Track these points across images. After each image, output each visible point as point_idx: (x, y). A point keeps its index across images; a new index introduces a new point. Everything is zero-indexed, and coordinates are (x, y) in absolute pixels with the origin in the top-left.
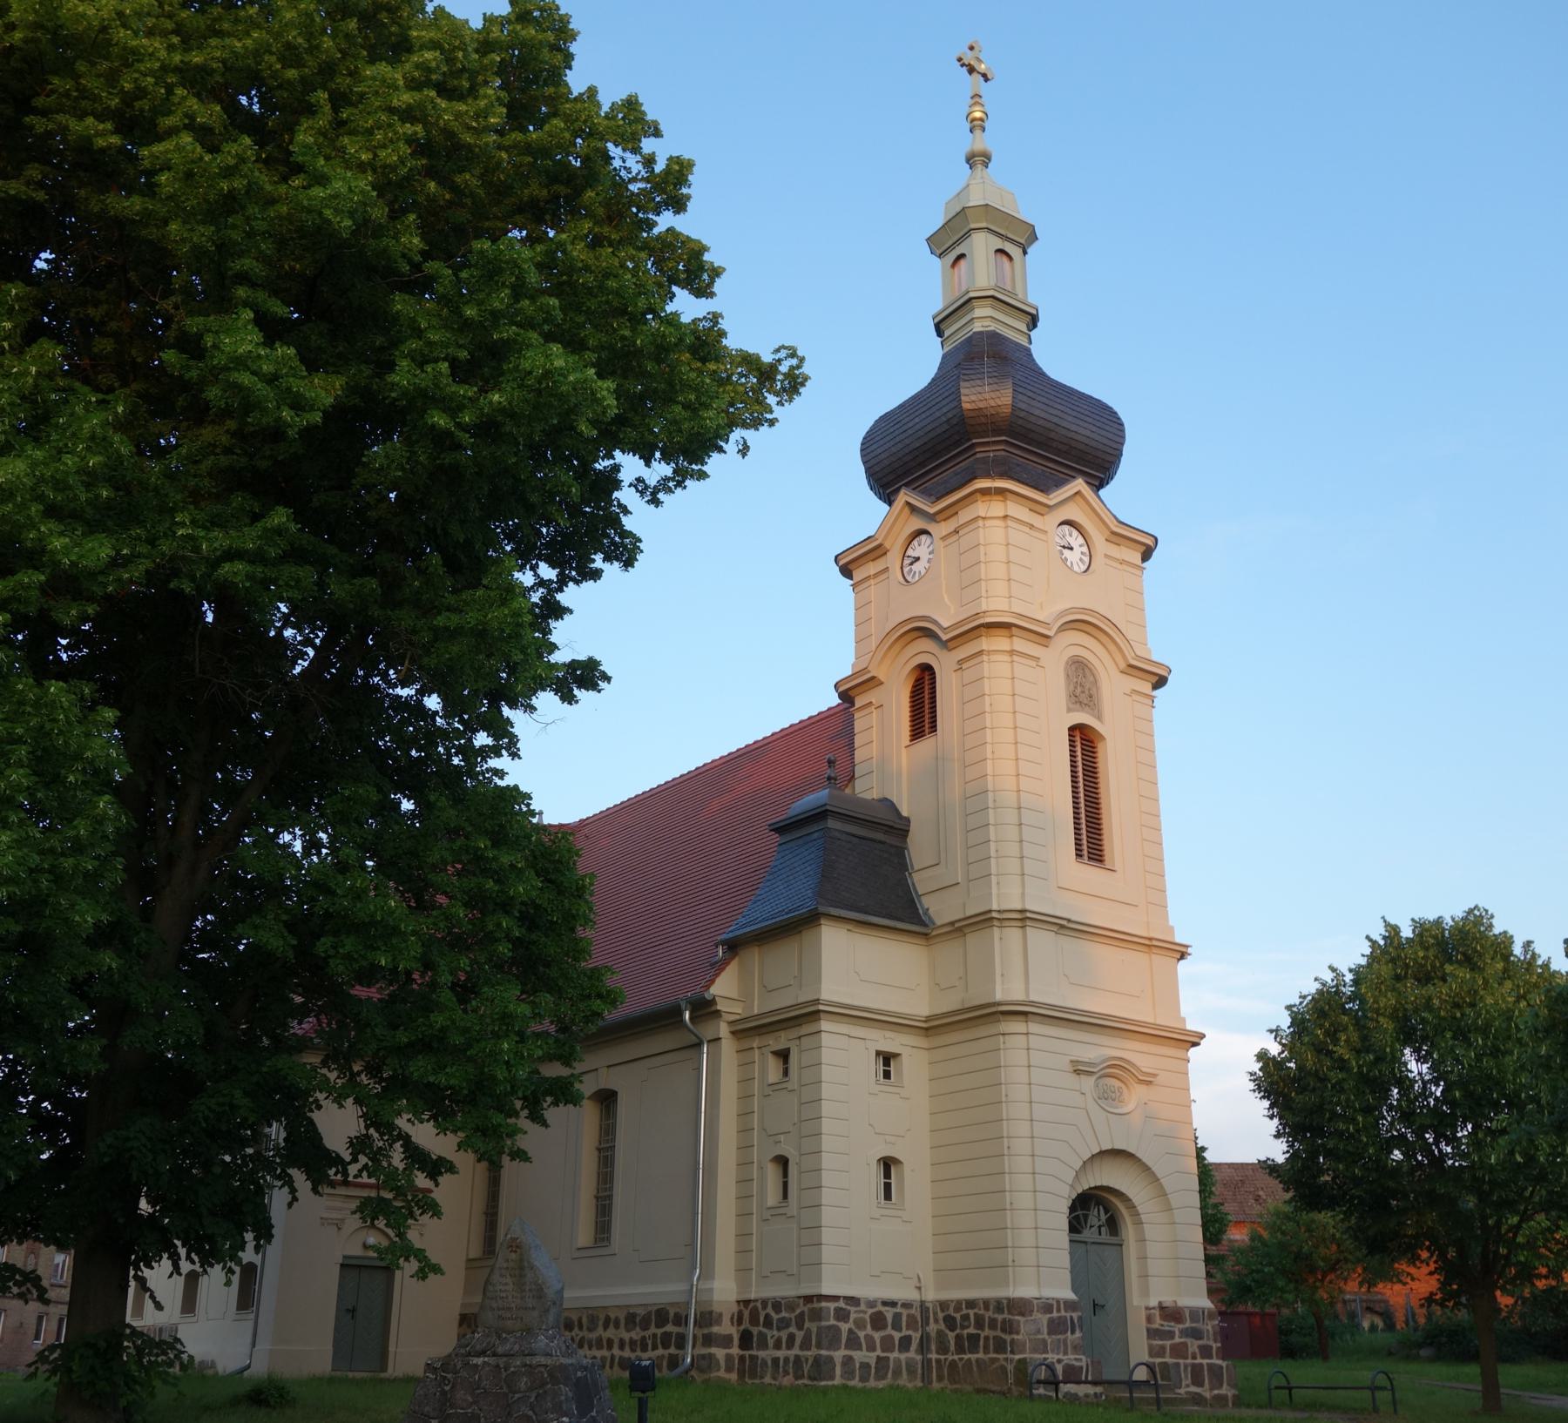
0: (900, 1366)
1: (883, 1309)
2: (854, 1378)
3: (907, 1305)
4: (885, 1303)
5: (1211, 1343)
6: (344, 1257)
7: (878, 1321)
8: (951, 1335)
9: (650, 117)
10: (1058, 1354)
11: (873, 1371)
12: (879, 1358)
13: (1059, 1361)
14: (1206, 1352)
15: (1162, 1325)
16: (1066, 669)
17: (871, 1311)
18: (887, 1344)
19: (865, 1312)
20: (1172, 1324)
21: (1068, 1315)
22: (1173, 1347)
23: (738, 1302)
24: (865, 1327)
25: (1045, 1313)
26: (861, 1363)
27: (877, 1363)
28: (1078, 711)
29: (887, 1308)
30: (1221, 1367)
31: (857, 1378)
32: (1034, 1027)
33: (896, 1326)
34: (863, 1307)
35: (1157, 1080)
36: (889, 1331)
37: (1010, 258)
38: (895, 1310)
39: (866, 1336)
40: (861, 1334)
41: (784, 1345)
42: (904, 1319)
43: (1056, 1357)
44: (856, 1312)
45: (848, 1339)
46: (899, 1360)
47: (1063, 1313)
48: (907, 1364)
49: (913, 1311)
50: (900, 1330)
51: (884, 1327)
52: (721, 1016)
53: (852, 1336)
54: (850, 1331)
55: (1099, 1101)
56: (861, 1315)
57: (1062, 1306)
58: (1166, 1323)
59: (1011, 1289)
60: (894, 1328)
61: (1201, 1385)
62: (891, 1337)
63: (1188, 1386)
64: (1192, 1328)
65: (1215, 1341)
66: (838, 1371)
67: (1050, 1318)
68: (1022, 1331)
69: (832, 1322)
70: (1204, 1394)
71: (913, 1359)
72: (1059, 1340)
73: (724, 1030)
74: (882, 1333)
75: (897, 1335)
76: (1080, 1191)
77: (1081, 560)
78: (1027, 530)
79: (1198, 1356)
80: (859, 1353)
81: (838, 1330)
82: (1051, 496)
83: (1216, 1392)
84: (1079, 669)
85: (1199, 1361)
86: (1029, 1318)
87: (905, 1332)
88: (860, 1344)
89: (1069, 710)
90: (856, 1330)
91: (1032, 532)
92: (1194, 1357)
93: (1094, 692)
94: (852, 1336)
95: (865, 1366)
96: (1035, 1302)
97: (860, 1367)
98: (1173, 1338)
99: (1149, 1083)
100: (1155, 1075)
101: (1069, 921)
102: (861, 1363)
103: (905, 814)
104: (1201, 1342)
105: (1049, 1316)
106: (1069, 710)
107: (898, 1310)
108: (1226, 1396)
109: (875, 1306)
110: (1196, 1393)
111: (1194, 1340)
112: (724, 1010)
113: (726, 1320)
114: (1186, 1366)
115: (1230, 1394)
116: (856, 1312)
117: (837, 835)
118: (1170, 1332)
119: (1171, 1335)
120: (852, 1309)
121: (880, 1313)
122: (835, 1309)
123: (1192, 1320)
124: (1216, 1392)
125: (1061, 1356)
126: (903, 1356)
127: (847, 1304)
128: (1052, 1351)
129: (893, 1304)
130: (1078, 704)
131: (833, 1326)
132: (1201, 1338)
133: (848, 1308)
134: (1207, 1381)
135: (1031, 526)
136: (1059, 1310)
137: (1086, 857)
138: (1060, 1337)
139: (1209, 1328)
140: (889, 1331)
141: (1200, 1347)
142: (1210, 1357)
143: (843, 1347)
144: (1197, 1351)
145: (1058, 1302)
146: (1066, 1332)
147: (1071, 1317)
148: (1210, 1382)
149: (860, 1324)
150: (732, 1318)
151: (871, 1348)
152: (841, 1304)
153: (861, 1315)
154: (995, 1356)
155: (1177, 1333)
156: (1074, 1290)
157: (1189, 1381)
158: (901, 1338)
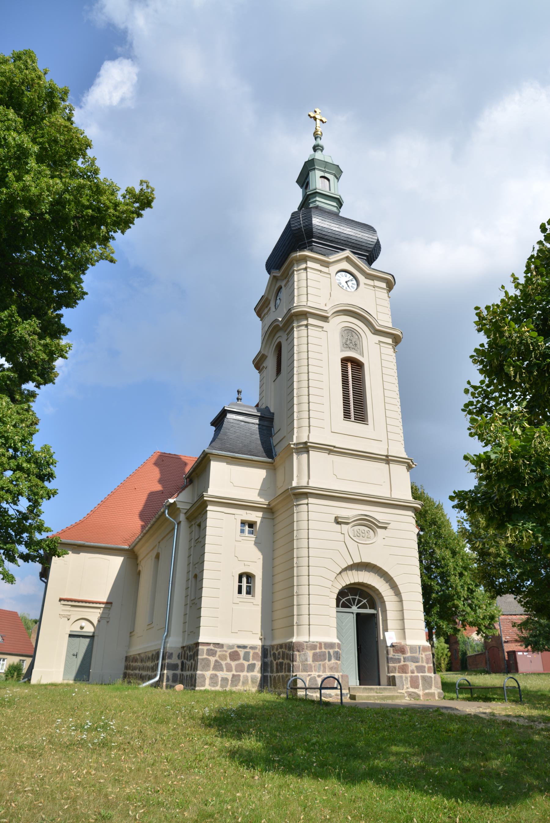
0: (247, 680)
1: (238, 650)
2: (217, 685)
3: (252, 648)
4: (239, 647)
5: (424, 664)
6: (71, 631)
7: (234, 656)
8: (275, 663)
9: (526, 269)
10: (319, 672)
11: (230, 682)
12: (233, 675)
13: (319, 676)
14: (421, 669)
15: (394, 656)
16: (341, 332)
17: (230, 651)
18: (240, 668)
19: (226, 651)
20: (399, 655)
21: (327, 651)
22: (399, 667)
23: (183, 647)
24: (226, 659)
25: (311, 650)
26: (222, 678)
27: (232, 678)
28: (347, 351)
29: (241, 649)
30: (431, 677)
31: (219, 685)
32: (311, 500)
33: (246, 658)
34: (225, 649)
35: (389, 527)
36: (242, 661)
37: (328, 180)
38: (246, 650)
39: (226, 664)
40: (223, 663)
41: (246, 669)
42: (251, 654)
43: (317, 674)
44: (220, 651)
45: (215, 665)
46: (247, 677)
47: (323, 650)
48: (252, 678)
49: (257, 651)
50: (248, 661)
51: (239, 659)
52: (180, 511)
53: (217, 664)
54: (216, 661)
55: (353, 538)
56: (224, 653)
57: (323, 646)
58: (396, 654)
59: (295, 637)
60: (244, 659)
61: (417, 687)
62: (242, 665)
63: (408, 688)
64: (411, 656)
65: (427, 663)
66: (207, 681)
67: (314, 653)
68: (298, 660)
69: (205, 656)
70: (418, 692)
71: (255, 676)
72: (320, 664)
73: (182, 517)
74: (237, 662)
75: (246, 664)
76: (340, 587)
77: (339, 280)
78: (319, 273)
79: (415, 672)
80: (221, 673)
81: (209, 661)
82: (330, 257)
83: (427, 691)
84: (349, 331)
85: (416, 674)
86: (302, 653)
87: (251, 662)
88: (223, 668)
89: (342, 351)
90: (220, 661)
91: (321, 274)
92: (413, 672)
93: (358, 342)
94: (217, 664)
95: (225, 680)
96: (305, 644)
97: (221, 680)
98: (400, 662)
99: (385, 528)
100: (389, 524)
101: (334, 447)
102: (222, 678)
103: (272, 411)
104: (417, 664)
105: (313, 651)
106: (342, 351)
107: (248, 650)
108: (434, 693)
109: (233, 648)
110: (413, 692)
111: (412, 663)
112: (181, 507)
113: (175, 656)
114: (406, 678)
115: (436, 693)
116: (220, 651)
117: (232, 421)
118: (398, 659)
119: (399, 661)
120: (218, 650)
121: (236, 652)
122: (207, 650)
123: (411, 652)
124: (427, 691)
125: (321, 674)
126: (250, 674)
127: (214, 647)
128: (315, 671)
129: (244, 647)
130: (348, 349)
131: (205, 658)
132: (417, 662)
133: (216, 649)
134: (421, 685)
135: (321, 271)
136: (321, 648)
137: (353, 419)
138: (320, 663)
139: (423, 656)
140: (242, 661)
141: (416, 667)
142: (424, 672)
143: (211, 669)
144: (415, 669)
145: (320, 644)
146: (325, 660)
147: (329, 652)
148: (423, 686)
149: (223, 657)
150: (179, 656)
151: (229, 669)
152: (211, 647)
153: (224, 653)
154: (214, 672)
155: (402, 659)
156: (338, 638)
157: (409, 685)
158: (249, 665)
